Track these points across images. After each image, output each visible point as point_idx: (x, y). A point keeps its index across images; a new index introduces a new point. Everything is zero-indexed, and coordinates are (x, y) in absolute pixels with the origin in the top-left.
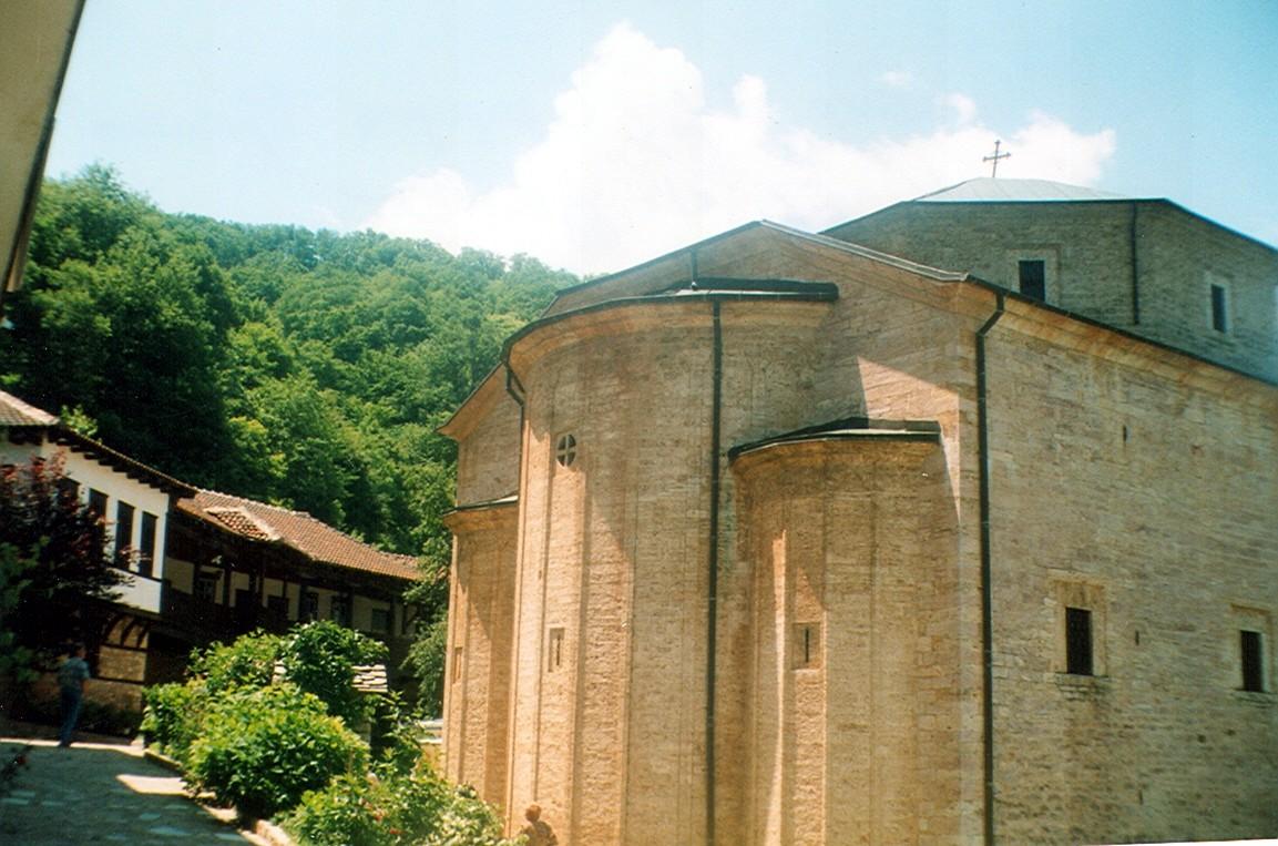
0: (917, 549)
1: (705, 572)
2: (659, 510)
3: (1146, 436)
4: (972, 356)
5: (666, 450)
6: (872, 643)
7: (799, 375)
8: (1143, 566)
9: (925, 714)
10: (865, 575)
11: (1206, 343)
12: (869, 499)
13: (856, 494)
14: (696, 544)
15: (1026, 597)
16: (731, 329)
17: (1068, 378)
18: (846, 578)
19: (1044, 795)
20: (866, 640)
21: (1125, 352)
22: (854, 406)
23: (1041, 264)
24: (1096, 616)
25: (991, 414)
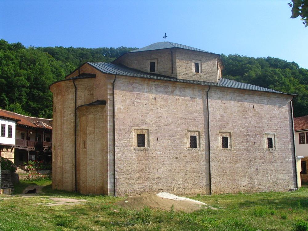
1: (74, 132)
2: (67, 120)
4: (112, 87)
15: (126, 133)
16: (76, 85)
17: (139, 89)
19: (131, 170)
21: (155, 82)
23: (154, 62)
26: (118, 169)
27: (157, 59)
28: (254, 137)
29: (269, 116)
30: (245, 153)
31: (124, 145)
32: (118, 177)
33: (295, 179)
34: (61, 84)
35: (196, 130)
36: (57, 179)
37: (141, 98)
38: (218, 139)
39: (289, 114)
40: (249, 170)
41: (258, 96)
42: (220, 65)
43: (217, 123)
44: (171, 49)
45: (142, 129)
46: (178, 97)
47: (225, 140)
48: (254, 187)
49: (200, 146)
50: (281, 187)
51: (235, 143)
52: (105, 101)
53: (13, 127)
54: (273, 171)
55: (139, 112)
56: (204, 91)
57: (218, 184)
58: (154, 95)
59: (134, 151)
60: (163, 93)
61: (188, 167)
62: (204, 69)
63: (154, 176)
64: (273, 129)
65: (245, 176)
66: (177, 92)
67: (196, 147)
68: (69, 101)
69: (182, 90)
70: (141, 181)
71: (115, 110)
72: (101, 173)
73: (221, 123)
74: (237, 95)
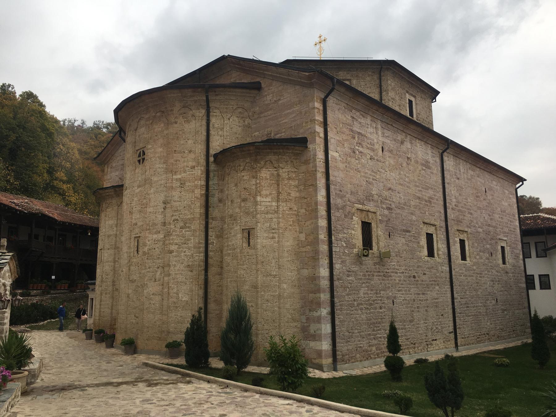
0: (298, 194)
3: (391, 151)
4: (321, 108)
5: (185, 155)
6: (279, 237)
7: (244, 122)
8: (390, 204)
9: (303, 269)
10: (275, 206)
11: (175, 396)
12: (276, 172)
13: (270, 170)
14: (199, 197)
15: (346, 216)
17: (360, 123)
18: (266, 208)
20: (276, 235)
22: (269, 134)
24: (374, 225)
25: (330, 135)
37: (364, 144)
45: (368, 211)
55: (363, 174)
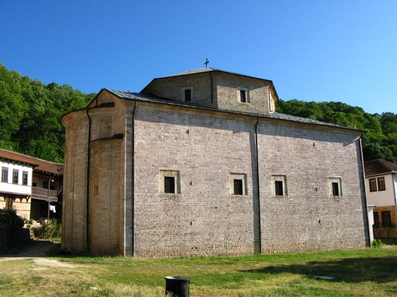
2: (78, 160)
4: (131, 117)
17: (167, 119)
19: (155, 223)
21: (188, 111)
26: (138, 222)
27: (193, 85)
28: (316, 182)
29: (333, 156)
30: (304, 201)
31: (147, 191)
32: (138, 232)
33: (367, 233)
34: (73, 115)
35: (242, 171)
36: (66, 235)
37: (170, 131)
38: (270, 184)
39: (357, 154)
40: (310, 223)
41: (320, 132)
42: (272, 95)
43: (268, 164)
44: (210, 72)
46: (219, 131)
47: (279, 185)
48: (317, 244)
49: (246, 193)
50: (349, 244)
51: (291, 187)
52: (123, 134)
53: (28, 173)
54: (339, 224)
56: (252, 124)
57: (270, 241)
58: (187, 128)
59: (160, 199)
60: (198, 126)
61: (232, 219)
62: (252, 98)
63: (186, 230)
64: (339, 172)
65: (304, 230)
66: (217, 124)
67: (241, 194)
68: (82, 136)
69: (223, 122)
70: (169, 238)
71: (135, 146)
72: (116, 227)
73: (274, 164)
74: (294, 129)
